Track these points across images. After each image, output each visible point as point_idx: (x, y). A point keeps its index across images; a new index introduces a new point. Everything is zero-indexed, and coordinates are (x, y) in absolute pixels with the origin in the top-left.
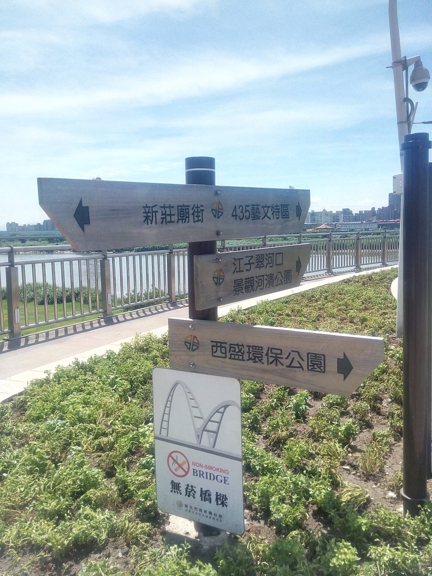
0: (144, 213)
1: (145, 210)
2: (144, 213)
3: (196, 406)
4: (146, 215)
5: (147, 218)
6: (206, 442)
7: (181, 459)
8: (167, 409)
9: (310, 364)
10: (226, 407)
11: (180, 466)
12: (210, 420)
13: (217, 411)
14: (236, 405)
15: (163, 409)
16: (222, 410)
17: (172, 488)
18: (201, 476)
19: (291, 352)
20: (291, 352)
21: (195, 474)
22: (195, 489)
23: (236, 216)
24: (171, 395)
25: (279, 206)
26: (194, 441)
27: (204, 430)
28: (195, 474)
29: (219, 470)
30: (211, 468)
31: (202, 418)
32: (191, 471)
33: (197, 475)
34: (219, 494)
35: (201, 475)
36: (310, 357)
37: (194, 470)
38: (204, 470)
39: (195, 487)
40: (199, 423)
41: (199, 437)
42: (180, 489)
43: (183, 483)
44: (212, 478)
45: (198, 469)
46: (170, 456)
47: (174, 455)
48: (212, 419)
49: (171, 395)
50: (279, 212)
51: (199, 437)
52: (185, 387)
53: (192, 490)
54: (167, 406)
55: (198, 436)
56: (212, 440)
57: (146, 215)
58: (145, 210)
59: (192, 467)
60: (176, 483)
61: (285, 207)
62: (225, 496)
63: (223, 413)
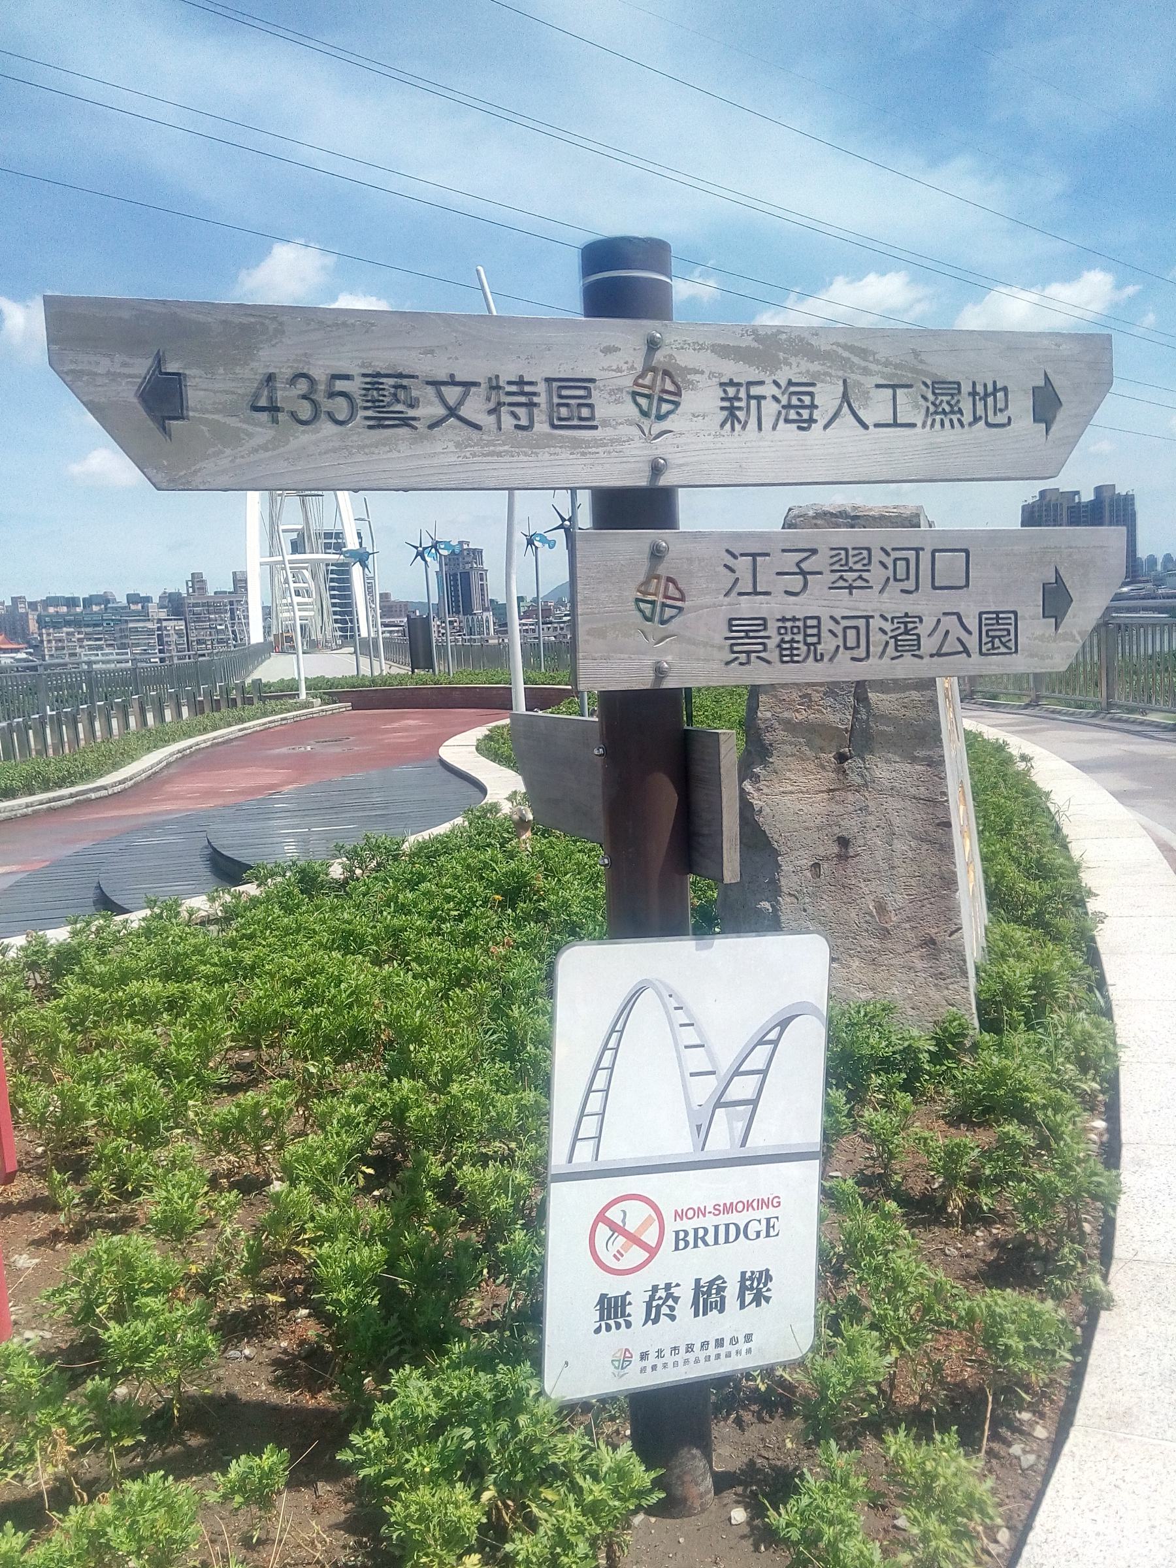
0: (722, 399)
1: (725, 391)
2: (722, 399)
3: (699, 1042)
4: (726, 404)
5: (731, 414)
6: (721, 1141)
7: (635, 1216)
8: (602, 1076)
9: (985, 639)
10: (784, 1024)
11: (634, 1239)
12: (737, 1073)
13: (761, 1042)
14: (815, 1011)
15: (589, 1075)
16: (772, 1036)
17: (601, 1319)
18: (700, 1242)
19: (966, 427)
20: (966, 427)
21: (682, 1244)
22: (676, 1291)
23: (273, 409)
24: (617, 1028)
25: (799, 620)
26: (682, 1146)
27: (719, 1104)
28: (682, 1244)
29: (755, 1204)
30: (729, 1208)
31: (713, 1073)
32: (669, 1238)
33: (686, 1246)
34: (748, 1274)
35: (700, 1239)
36: (984, 622)
37: (677, 1233)
38: (709, 1222)
39: (678, 1285)
40: (703, 1090)
41: (702, 1130)
42: (628, 1309)
43: (637, 1290)
44: (732, 1236)
45: (689, 1225)
46: (601, 1218)
47: (614, 1214)
48: (743, 1068)
49: (617, 1028)
50: (531, 405)
51: (702, 1130)
52: (666, 994)
53: (670, 1296)
54: (609, 1046)
55: (699, 1127)
56: (740, 1126)
57: (726, 404)
58: (725, 391)
59: (671, 1226)
60: (616, 1298)
61: (505, 625)
62: (767, 1270)
63: (775, 1043)
